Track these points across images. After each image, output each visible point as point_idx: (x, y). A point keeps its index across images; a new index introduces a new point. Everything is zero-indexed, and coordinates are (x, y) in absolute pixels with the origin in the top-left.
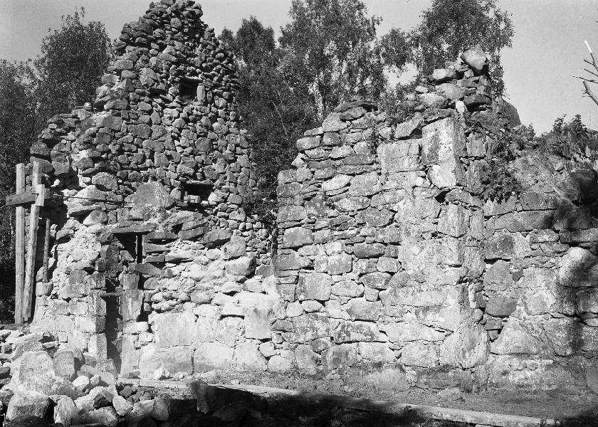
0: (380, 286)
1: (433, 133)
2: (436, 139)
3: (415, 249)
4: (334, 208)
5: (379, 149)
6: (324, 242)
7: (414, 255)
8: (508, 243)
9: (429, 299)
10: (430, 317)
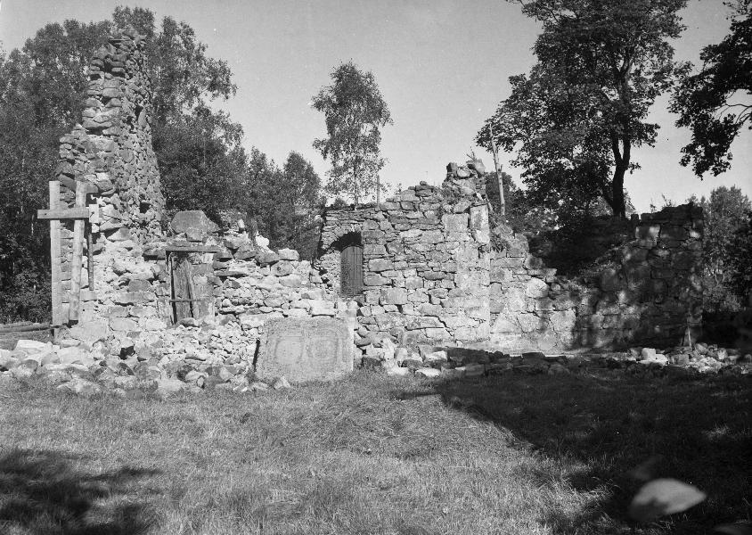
0: (442, 296)
1: (477, 212)
2: (479, 216)
3: (466, 276)
4: (409, 248)
5: (443, 218)
6: (403, 269)
7: (465, 280)
8: (501, 274)
9: (473, 303)
10: (473, 313)
